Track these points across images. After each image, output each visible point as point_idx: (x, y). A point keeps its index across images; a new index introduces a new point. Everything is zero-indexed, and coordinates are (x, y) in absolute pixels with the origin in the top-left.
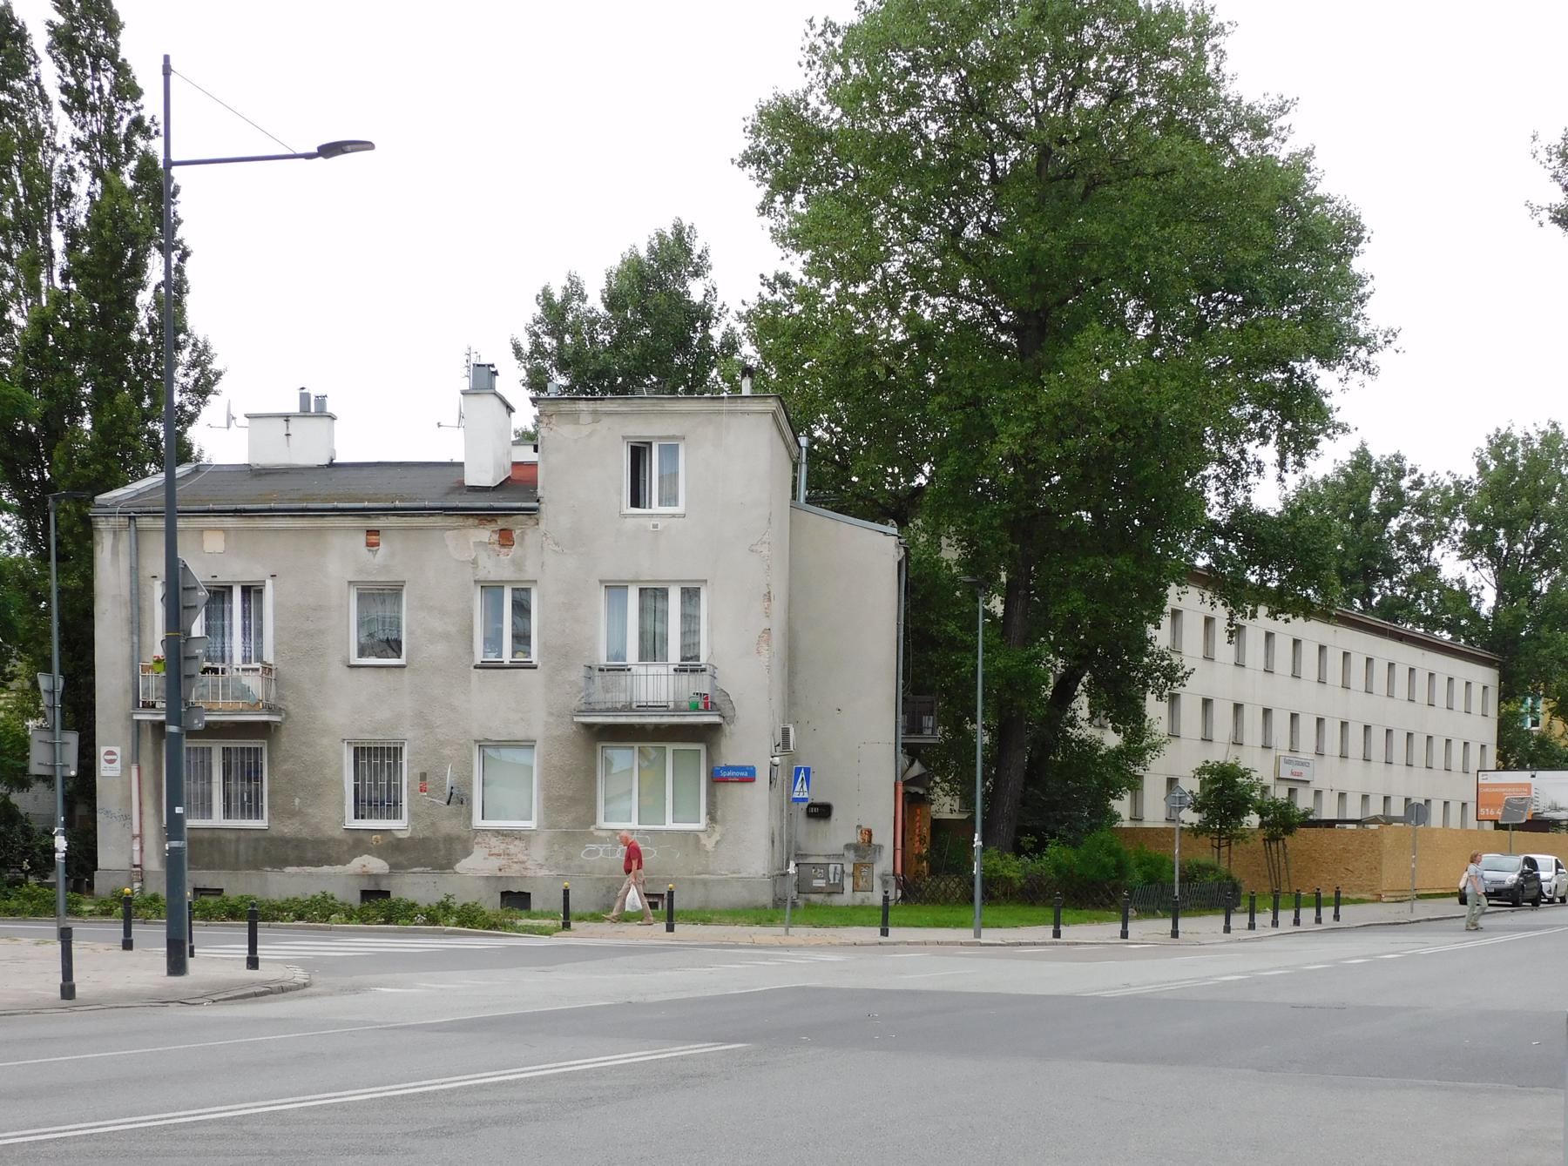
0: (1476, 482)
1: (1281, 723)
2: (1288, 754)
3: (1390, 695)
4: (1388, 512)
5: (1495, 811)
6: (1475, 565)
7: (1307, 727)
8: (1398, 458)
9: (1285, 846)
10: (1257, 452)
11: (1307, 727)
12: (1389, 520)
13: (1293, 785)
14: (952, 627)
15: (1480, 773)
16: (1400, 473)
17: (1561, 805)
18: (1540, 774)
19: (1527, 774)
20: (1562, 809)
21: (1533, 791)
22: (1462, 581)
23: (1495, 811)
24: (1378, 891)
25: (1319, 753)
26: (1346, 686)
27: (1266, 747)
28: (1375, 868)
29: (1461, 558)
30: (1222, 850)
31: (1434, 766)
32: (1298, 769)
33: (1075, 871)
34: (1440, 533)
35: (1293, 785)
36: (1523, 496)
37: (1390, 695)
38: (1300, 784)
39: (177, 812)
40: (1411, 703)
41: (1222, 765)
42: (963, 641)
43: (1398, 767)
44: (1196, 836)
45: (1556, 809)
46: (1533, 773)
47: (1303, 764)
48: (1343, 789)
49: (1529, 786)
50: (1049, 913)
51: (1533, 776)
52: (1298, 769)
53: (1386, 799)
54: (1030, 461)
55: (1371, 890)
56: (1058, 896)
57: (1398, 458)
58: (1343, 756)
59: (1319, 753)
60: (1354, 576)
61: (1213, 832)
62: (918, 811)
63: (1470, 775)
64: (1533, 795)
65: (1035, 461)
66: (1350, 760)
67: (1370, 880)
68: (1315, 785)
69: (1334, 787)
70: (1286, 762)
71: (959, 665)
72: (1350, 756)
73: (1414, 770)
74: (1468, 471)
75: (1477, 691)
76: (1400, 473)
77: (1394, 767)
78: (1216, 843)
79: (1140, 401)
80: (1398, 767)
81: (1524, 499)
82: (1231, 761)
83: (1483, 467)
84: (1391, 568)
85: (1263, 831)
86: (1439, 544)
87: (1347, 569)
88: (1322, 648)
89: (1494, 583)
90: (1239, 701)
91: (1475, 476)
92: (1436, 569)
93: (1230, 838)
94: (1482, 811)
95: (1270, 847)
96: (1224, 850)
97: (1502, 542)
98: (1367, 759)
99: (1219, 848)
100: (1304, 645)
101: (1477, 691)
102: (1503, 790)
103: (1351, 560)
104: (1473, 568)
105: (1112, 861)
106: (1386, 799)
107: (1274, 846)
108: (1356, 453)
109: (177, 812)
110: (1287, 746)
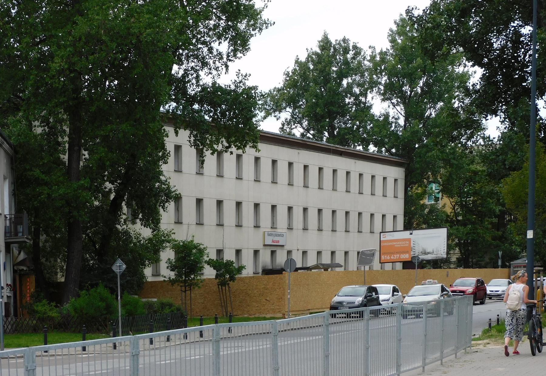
0: (391, 51)
1: (266, 211)
2: (270, 230)
3: (334, 189)
4: (342, 75)
5: (390, 257)
6: (393, 103)
7: (282, 212)
8: (344, 40)
9: (229, 287)
10: (218, 48)
11: (282, 212)
12: (343, 80)
13: (273, 249)
14: (37, 172)
15: (382, 234)
16: (346, 51)
17: (428, 250)
18: (415, 232)
19: (408, 232)
20: (429, 253)
21: (412, 243)
22: (387, 116)
23: (390, 257)
24: (283, 312)
25: (290, 228)
26: (306, 186)
27: (257, 227)
28: (281, 298)
29: (383, 100)
30: (187, 292)
31: (363, 231)
32: (276, 239)
33: (84, 311)
34: (373, 84)
35: (273, 249)
36: (418, 57)
37: (334, 189)
38: (278, 248)
39: (532, 237)
40: (348, 193)
41: (184, 242)
42: (43, 180)
43: (341, 232)
44: (172, 285)
45: (426, 253)
46: (411, 232)
47: (279, 235)
48: (305, 249)
49: (409, 240)
50: (41, 337)
51: (411, 234)
52: (276, 239)
53: (333, 253)
54: (71, 72)
55: (279, 311)
56: (84, 327)
57: (344, 40)
58: (305, 229)
59: (290, 228)
60: (323, 117)
61: (181, 282)
62: (28, 280)
63: (375, 234)
64: (412, 245)
65: (75, 71)
66: (309, 231)
67: (278, 305)
68: (288, 247)
69: (299, 248)
70: (269, 235)
71: (40, 194)
72: (309, 228)
73: (350, 234)
74: (384, 45)
75: (390, 183)
76: (346, 51)
77: (338, 234)
78: (183, 289)
79: (128, 29)
80: (341, 232)
81: (419, 59)
82: (190, 239)
83: (393, 41)
84: (343, 110)
85: (218, 280)
86: (370, 92)
87: (318, 113)
88: (290, 164)
89: (403, 113)
90: (239, 200)
91: (389, 48)
92: (370, 107)
93: (190, 286)
94: (383, 257)
95: (222, 289)
96: (188, 292)
97: (406, 88)
98: (320, 230)
99: (185, 291)
100: (279, 163)
101: (390, 183)
102: (395, 243)
103: (320, 108)
104: (391, 106)
105: (102, 305)
106: (333, 253)
107: (224, 288)
108: (322, 41)
109: (532, 237)
110: (269, 224)
